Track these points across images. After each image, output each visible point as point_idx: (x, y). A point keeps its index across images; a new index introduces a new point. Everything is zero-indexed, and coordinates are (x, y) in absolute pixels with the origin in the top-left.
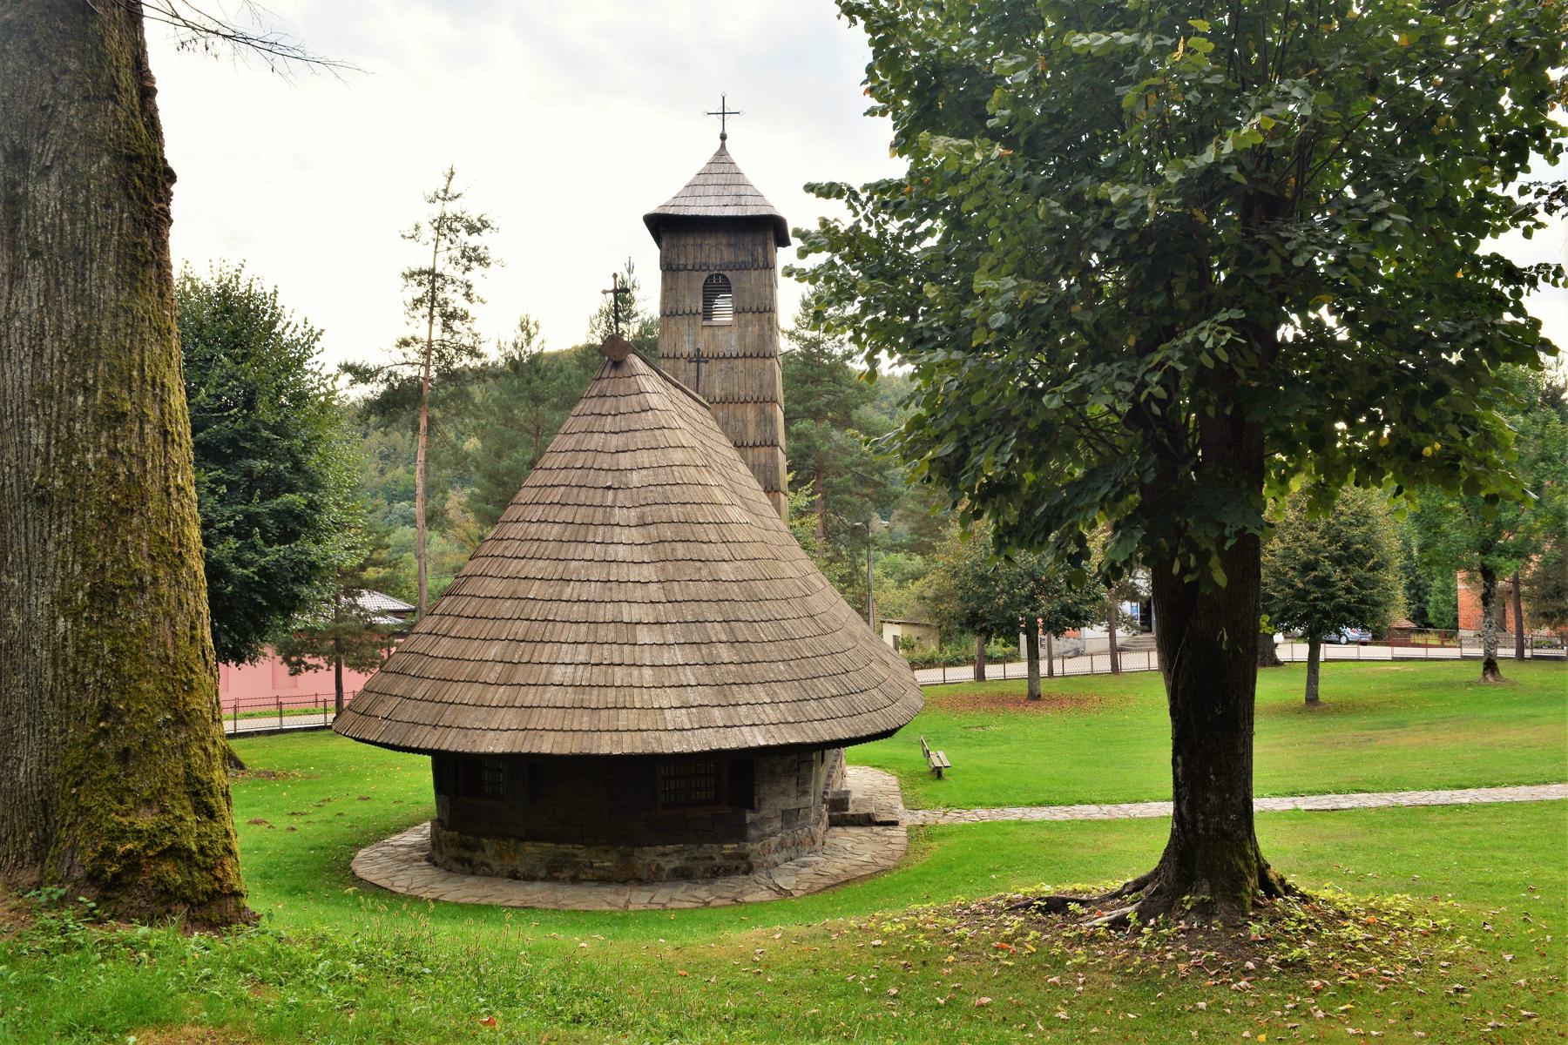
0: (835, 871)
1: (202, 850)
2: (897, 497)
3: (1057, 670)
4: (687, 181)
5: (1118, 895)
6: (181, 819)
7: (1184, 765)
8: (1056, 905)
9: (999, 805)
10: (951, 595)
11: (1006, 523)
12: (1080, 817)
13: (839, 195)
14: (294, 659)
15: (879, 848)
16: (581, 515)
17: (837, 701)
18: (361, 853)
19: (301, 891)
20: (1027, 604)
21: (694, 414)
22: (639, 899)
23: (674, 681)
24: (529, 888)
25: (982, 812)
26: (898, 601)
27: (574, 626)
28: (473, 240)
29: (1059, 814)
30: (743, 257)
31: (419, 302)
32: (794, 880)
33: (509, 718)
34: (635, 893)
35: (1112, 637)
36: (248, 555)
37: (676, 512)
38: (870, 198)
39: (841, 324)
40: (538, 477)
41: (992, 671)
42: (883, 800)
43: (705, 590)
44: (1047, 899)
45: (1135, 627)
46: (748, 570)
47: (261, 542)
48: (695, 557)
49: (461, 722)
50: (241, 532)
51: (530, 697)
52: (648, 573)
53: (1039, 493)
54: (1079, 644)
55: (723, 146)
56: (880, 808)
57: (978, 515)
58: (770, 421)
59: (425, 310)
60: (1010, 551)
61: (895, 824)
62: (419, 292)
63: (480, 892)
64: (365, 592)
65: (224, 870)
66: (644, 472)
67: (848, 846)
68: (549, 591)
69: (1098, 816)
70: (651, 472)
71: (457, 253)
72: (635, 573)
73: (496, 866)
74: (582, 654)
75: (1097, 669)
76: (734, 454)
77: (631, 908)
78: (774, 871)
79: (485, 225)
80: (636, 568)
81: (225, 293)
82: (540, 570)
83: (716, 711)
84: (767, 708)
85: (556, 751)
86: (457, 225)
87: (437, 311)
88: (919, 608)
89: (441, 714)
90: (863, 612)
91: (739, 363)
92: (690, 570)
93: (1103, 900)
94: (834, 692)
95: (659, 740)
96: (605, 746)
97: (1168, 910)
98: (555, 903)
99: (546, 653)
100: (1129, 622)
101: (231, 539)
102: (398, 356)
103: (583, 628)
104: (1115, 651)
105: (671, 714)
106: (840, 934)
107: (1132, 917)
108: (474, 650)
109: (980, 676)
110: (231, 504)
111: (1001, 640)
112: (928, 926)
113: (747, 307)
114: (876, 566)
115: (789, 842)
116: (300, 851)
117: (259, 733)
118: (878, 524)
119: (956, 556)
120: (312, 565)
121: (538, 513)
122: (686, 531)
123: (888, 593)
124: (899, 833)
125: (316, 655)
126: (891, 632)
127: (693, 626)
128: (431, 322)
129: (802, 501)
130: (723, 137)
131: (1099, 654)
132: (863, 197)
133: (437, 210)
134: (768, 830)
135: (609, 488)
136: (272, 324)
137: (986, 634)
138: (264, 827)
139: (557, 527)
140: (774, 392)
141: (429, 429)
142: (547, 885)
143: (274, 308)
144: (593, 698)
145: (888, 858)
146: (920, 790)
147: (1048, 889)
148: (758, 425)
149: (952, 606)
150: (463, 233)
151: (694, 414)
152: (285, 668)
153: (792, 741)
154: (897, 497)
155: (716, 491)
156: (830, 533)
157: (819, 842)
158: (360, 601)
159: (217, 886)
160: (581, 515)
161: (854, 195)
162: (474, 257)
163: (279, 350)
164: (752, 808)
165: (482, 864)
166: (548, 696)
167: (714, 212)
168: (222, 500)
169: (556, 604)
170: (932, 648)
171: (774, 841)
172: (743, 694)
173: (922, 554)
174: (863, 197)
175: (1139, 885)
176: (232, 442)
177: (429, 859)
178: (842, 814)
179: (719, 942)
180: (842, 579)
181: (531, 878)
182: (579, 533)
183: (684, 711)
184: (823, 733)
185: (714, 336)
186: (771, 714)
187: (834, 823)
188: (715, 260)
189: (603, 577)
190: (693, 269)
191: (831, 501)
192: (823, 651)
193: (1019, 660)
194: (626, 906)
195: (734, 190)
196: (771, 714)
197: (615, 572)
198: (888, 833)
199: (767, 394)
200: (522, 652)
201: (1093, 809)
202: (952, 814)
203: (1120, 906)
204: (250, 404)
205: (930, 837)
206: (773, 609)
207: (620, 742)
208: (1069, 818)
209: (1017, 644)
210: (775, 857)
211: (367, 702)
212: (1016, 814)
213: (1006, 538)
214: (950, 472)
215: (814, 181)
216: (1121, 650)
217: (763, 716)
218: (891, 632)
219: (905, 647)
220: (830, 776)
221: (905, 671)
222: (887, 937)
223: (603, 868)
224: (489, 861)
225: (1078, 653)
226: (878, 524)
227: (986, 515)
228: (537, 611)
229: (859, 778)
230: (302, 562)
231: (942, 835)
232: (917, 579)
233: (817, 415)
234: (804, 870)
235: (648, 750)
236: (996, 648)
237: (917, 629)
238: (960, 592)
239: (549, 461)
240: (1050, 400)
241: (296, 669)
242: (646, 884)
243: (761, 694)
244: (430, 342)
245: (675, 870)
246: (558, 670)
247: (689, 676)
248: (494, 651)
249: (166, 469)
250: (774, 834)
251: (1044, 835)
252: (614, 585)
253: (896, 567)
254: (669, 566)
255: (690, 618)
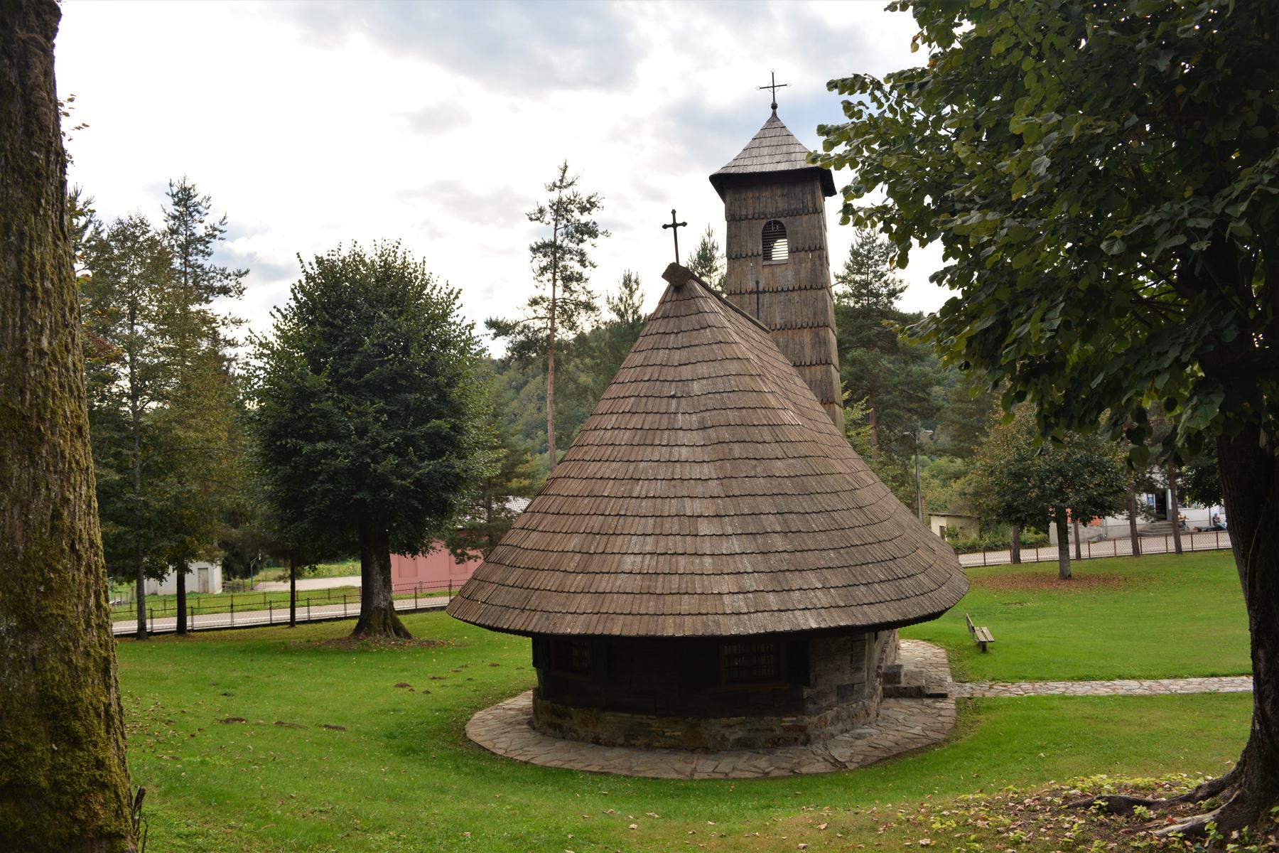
0: (888, 744)
1: (56, 786)
2: (938, 409)
3: (1084, 553)
4: (744, 146)
5: (1189, 798)
6: (28, 748)
7: (1268, 660)
8: (1119, 806)
9: (1042, 679)
10: (988, 490)
11: (1051, 404)
12: (1121, 692)
13: (863, 89)
14: (459, 551)
15: (929, 721)
16: (650, 421)
17: (886, 586)
18: (477, 715)
19: (414, 752)
20: (1056, 497)
21: (754, 335)
22: (704, 767)
23: (731, 569)
24: (609, 754)
25: (1026, 685)
26: (943, 498)
27: (643, 520)
28: (585, 218)
29: (1101, 689)
30: (795, 205)
31: (544, 270)
32: (848, 752)
33: (584, 603)
34: (701, 762)
35: (1133, 524)
36: (405, 470)
37: (732, 416)
38: (892, 88)
39: (869, 217)
40: (614, 390)
41: (1027, 555)
42: (933, 672)
43: (761, 485)
44: (1108, 799)
45: (1152, 515)
46: (800, 467)
47: (415, 459)
48: (751, 456)
49: (543, 606)
50: (399, 451)
51: (604, 584)
52: (707, 471)
53: (1087, 368)
54: (1102, 531)
55: (774, 114)
56: (929, 680)
57: (1021, 397)
58: (824, 343)
59: (549, 275)
60: (1057, 432)
61: (944, 696)
62: (545, 262)
63: (566, 756)
64: (511, 498)
65: (88, 809)
66: (704, 382)
67: (901, 717)
68: (622, 489)
69: (1140, 691)
70: (710, 381)
71: (571, 229)
72: (696, 472)
73: (582, 732)
74: (649, 544)
75: (1119, 552)
76: (793, 371)
77: (696, 776)
78: (831, 742)
79: (593, 205)
80: (697, 467)
81: (387, 266)
82: (613, 471)
83: (771, 597)
84: (819, 593)
85: (625, 633)
86: (571, 207)
87: (558, 275)
88: (961, 503)
89: (528, 599)
90: (912, 505)
91: (795, 295)
92: (745, 468)
93: (1172, 803)
94: (883, 577)
95: (717, 623)
96: (669, 628)
97: (1253, 821)
98: (629, 769)
99: (618, 544)
100: (1147, 511)
101: (391, 456)
102: (530, 312)
103: (651, 521)
104: (1135, 536)
105: (735, 601)
106: (888, 827)
107: (1211, 828)
108: (557, 543)
109: (1016, 559)
110: (392, 430)
111: (1033, 528)
112: (980, 823)
113: (800, 247)
114: (923, 468)
115: (844, 714)
116: (428, 713)
117: (434, 609)
118: (924, 435)
119: (992, 457)
120: (457, 476)
121: (612, 421)
122: (742, 433)
123: (935, 492)
124: (949, 705)
125: (474, 548)
126: (937, 524)
127: (749, 519)
128: (554, 285)
129: (857, 414)
130: (774, 107)
131: (1120, 539)
132: (887, 87)
133: (555, 196)
134: (824, 704)
135: (673, 397)
136: (424, 287)
137: (1021, 523)
138: (406, 690)
139: (628, 433)
140: (826, 318)
141: (556, 369)
142: (624, 751)
143: (424, 274)
144: (660, 585)
145: (938, 731)
146: (968, 663)
147: (1106, 782)
148: (813, 347)
149: (992, 501)
150: (576, 214)
151: (754, 335)
152: (453, 558)
153: (842, 624)
154: (938, 409)
155: (770, 397)
156: (883, 443)
157: (873, 714)
158: (508, 505)
159: (76, 830)
160: (650, 421)
161: (878, 86)
162: (588, 231)
163: (429, 303)
164: (808, 685)
165: (571, 730)
166: (619, 582)
167: (768, 168)
168: (385, 425)
169: (627, 501)
170: (974, 536)
171: (830, 714)
172: (796, 581)
173: (962, 457)
174: (887, 87)
175: (1214, 790)
176: (392, 381)
177: (530, 723)
178: (898, 687)
179: (764, 828)
180: (894, 478)
181: (611, 745)
182: (646, 436)
183: (741, 596)
184: (873, 615)
185: (773, 274)
186: (822, 598)
187: (888, 694)
188: (771, 209)
189: (669, 476)
190: (753, 218)
191: (883, 416)
192: (871, 540)
193: (1049, 545)
194: (692, 775)
195: (784, 149)
196: (822, 598)
197: (678, 471)
198: (938, 705)
199: (821, 319)
200: (598, 544)
201: (1133, 684)
202: (998, 687)
203: (1194, 812)
204: (406, 350)
205: (977, 710)
206: (824, 502)
207: (682, 626)
208: (1112, 693)
209: (1047, 532)
210: (831, 729)
211: (472, 588)
212: (1058, 688)
213: (1050, 420)
214: (986, 350)
215: (837, 76)
216: (1141, 535)
217: (815, 601)
218: (937, 524)
219: (950, 535)
220: (884, 651)
221: (950, 556)
222: (936, 834)
223: (674, 737)
224: (576, 728)
225: (1101, 539)
226: (924, 435)
227: (1029, 397)
228: (611, 507)
229: (911, 651)
230: (449, 474)
231: (989, 708)
232: (958, 478)
233: (868, 344)
234: (859, 742)
235: (709, 632)
236: (1028, 535)
237: (959, 520)
238: (997, 488)
239: (624, 375)
240: (1110, 247)
241: (461, 559)
242: (713, 753)
243: (813, 580)
244: (554, 299)
245: (738, 740)
246: (629, 560)
247: (746, 564)
248: (574, 542)
249: (22, 329)
250: (830, 707)
251: (1088, 710)
252: (678, 482)
253: (941, 471)
254: (728, 464)
255: (746, 511)
